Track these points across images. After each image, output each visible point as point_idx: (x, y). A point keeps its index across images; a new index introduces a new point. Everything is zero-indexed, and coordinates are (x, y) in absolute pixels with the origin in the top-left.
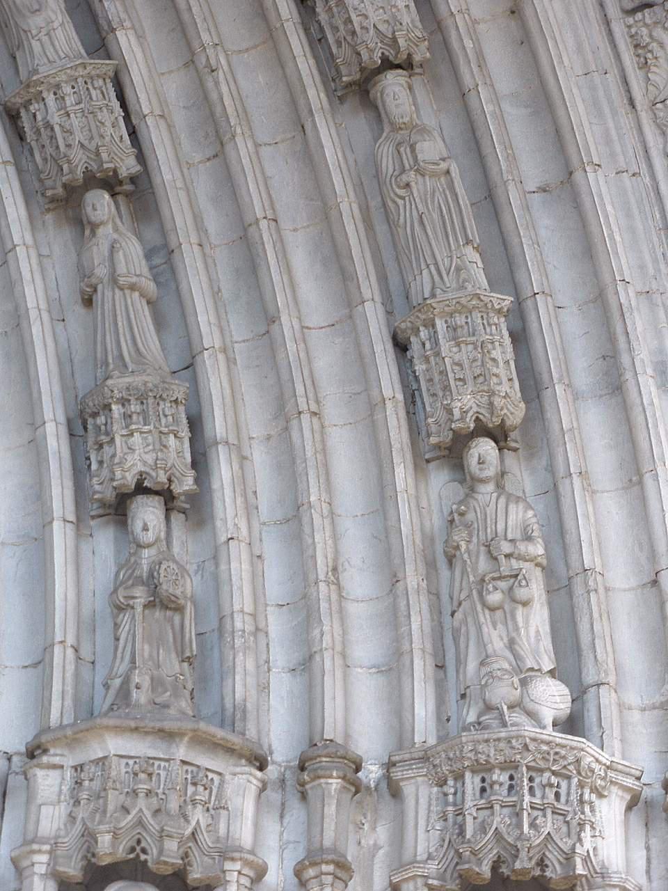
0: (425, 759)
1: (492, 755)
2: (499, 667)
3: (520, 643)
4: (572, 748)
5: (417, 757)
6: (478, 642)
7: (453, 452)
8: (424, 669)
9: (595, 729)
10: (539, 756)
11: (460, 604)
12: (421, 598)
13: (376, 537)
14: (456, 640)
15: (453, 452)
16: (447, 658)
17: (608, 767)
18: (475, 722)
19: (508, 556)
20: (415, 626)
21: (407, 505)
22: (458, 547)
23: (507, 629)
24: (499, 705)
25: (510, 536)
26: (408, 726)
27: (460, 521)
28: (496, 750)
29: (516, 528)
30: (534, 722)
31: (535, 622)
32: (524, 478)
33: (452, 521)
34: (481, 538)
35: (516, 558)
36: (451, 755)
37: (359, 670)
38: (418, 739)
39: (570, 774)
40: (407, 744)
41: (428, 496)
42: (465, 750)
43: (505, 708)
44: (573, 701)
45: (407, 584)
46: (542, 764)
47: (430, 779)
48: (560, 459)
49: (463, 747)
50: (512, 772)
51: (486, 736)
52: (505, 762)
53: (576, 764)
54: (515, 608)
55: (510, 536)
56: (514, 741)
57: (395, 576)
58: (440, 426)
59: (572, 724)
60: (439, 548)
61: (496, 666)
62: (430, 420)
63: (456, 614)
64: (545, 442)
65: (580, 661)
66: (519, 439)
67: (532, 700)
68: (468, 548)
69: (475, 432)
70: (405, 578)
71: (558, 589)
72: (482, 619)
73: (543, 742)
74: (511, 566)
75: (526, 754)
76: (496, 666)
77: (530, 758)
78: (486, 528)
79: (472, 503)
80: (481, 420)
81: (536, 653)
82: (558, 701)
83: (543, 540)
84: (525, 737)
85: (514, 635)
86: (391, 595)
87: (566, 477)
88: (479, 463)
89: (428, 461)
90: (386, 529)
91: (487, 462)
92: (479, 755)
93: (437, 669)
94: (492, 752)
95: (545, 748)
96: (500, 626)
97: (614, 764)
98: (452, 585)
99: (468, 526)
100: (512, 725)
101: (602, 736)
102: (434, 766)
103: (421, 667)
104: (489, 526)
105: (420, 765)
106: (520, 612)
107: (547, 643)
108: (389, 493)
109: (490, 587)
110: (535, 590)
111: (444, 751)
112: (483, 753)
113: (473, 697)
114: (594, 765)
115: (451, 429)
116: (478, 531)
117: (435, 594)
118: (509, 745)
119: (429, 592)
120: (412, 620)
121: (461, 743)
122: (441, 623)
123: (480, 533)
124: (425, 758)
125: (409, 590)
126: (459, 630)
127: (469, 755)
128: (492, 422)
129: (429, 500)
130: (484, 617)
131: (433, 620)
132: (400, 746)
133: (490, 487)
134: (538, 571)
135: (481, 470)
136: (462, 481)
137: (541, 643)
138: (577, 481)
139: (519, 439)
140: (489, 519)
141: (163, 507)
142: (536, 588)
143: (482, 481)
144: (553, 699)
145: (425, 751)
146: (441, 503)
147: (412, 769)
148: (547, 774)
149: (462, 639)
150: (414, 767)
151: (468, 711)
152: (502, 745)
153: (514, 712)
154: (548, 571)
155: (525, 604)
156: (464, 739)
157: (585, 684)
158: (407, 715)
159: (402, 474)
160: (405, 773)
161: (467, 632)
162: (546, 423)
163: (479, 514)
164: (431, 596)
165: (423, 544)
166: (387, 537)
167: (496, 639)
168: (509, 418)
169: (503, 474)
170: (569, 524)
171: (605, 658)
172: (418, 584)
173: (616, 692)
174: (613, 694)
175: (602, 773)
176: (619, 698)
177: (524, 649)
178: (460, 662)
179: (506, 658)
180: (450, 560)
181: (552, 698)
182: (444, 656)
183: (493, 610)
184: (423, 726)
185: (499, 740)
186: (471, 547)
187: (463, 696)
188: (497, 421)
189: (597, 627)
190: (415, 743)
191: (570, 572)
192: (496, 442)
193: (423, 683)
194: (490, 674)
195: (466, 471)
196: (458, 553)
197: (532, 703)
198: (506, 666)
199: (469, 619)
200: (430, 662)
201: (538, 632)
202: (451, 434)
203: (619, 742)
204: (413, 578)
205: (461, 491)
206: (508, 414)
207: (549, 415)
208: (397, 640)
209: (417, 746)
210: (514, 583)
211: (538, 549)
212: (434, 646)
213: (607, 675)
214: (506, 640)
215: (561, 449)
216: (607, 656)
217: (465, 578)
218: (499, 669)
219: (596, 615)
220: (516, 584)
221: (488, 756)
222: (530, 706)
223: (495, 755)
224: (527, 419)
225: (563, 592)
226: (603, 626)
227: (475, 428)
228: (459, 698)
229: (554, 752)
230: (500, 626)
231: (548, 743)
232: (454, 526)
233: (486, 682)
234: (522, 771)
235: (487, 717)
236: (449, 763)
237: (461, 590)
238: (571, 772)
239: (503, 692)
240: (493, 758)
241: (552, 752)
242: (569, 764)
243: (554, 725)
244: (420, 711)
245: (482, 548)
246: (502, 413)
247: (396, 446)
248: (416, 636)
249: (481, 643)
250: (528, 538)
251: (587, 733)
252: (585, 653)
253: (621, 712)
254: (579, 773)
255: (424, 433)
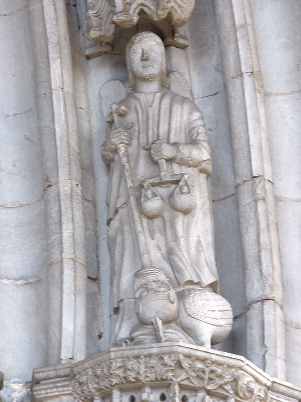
0: (71, 376)
1: (142, 372)
2: (155, 279)
3: (179, 253)
4: (230, 367)
5: (62, 374)
6: (134, 253)
7: (115, 48)
8: (75, 280)
9: (257, 348)
10: (193, 374)
11: (116, 211)
12: (74, 204)
13: (28, 139)
14: (111, 250)
15: (115, 48)
16: (101, 270)
17: (269, 388)
18: (128, 339)
19: (170, 161)
20: (67, 233)
21: (62, 103)
22: (116, 151)
23: (166, 239)
24: (153, 320)
25: (173, 139)
26: (55, 342)
27: (120, 123)
28: (146, 367)
29: (180, 131)
30: (190, 338)
31: (197, 232)
32: (191, 76)
33: (111, 123)
34: (142, 141)
35: (177, 163)
36: (99, 372)
37: (6, 282)
38: (65, 355)
39: (227, 394)
40: (53, 360)
41: (87, 95)
42: (113, 367)
43: (160, 323)
44: (235, 318)
45: (59, 188)
46: (196, 383)
47: (75, 398)
48: (231, 57)
49: (111, 363)
50: (164, 391)
51: (136, 352)
52: (157, 380)
53: (234, 383)
54: (176, 217)
55: (173, 139)
56: (166, 358)
57: (47, 180)
58: (101, 19)
59: (233, 341)
60: (97, 152)
61: (151, 278)
62: (91, 12)
63: (112, 222)
64: (216, 38)
65: (244, 275)
66: (188, 35)
67: (189, 315)
68: (127, 151)
69: (140, 27)
70: (58, 183)
71: (225, 198)
72: (139, 228)
73: (198, 359)
74: (173, 172)
75: (179, 371)
76: (151, 278)
77: (184, 376)
78: (148, 130)
79: (134, 103)
80: (146, 13)
81: (196, 265)
82: (218, 317)
83: (210, 144)
84: (178, 353)
85: (173, 245)
86: (42, 201)
87: (237, 77)
88: (143, 60)
89: (88, 58)
90: (40, 129)
91: (151, 59)
92: (129, 373)
93: (89, 281)
94: (143, 369)
95: (199, 365)
96: (158, 235)
97: (276, 385)
98: (109, 191)
99: (128, 128)
100: (166, 341)
101: (264, 356)
102: (81, 384)
103: (71, 279)
104: (150, 128)
105: (66, 383)
106: (180, 221)
107: (208, 254)
108: (43, 90)
109: (149, 193)
110: (198, 198)
111: (92, 368)
112: (133, 370)
113: (126, 312)
114: (253, 385)
115: (114, 23)
116: (139, 133)
117: (90, 201)
118: (161, 362)
119: (84, 199)
120: (64, 227)
121: (110, 359)
122: (96, 232)
123: (141, 135)
124: (71, 375)
125: (62, 195)
126: (114, 240)
127: (118, 372)
128: (157, 15)
129: (88, 99)
130: (141, 226)
131: (86, 229)
132: (46, 363)
133: (154, 86)
134: (202, 178)
135: (144, 67)
136: (124, 80)
137: (202, 255)
138: (247, 80)
139: (188, 35)
140: (151, 121)
141: (248, 313)
142: (199, 196)
143: (145, 79)
144: (214, 315)
145: (71, 368)
146: (100, 103)
147: (57, 387)
148: (201, 394)
149: (118, 249)
150: (59, 384)
151: (120, 327)
152: (153, 362)
153: (170, 327)
154: (214, 178)
155: (186, 212)
156: (113, 355)
157: (249, 300)
158: (54, 329)
159: (58, 70)
160: (49, 391)
161: (123, 242)
162: (218, 19)
163: (140, 115)
164: (86, 204)
165: (80, 148)
166: (40, 139)
167: (153, 249)
168: (176, 11)
169: (169, 72)
170: (238, 128)
171: (271, 271)
172: (72, 190)
173: (282, 308)
174: (279, 311)
175: (262, 395)
176: (285, 315)
177: (183, 259)
178: (115, 274)
179: (162, 270)
180: (109, 164)
181: (211, 313)
182: (99, 268)
183: (151, 217)
184: (70, 341)
185: (150, 356)
186: (131, 151)
187: (116, 310)
188: (163, 14)
189: (264, 238)
190: (61, 360)
191: (238, 180)
192: (163, 38)
193: (73, 297)
194: (146, 287)
195: (129, 69)
196: (116, 157)
197: (189, 318)
198: (162, 277)
199: (126, 228)
200: (82, 273)
201: (199, 243)
202: (112, 28)
203: (284, 363)
204: (66, 182)
205: (122, 90)
206: (176, 7)
207: (221, 10)
208: (47, 249)
209: (63, 362)
210: (175, 189)
211: (202, 154)
212: (87, 257)
213: (272, 289)
214: (164, 250)
215: (232, 47)
216: (273, 270)
217: (123, 182)
218: (154, 281)
219: (263, 225)
220: (177, 190)
221: (138, 373)
222: (187, 321)
223: (146, 372)
224: (196, 14)
225: (229, 201)
226: (270, 238)
227: (138, 21)
228: (112, 313)
229: (207, 372)
230: (158, 235)
231: (203, 360)
232: (113, 128)
233: (141, 295)
234: (174, 390)
235: (140, 332)
236: (97, 381)
237: (118, 197)
238: (227, 391)
239: (158, 306)
240: (143, 375)
241: (207, 370)
242: (226, 384)
243: (214, 343)
244: (68, 325)
245: (143, 152)
246: (169, 5)
247: (52, 39)
248: (67, 244)
249: (137, 253)
250: (193, 142)
251: (249, 352)
252: (250, 266)
253: (287, 330)
254: (237, 394)
255: (84, 28)
